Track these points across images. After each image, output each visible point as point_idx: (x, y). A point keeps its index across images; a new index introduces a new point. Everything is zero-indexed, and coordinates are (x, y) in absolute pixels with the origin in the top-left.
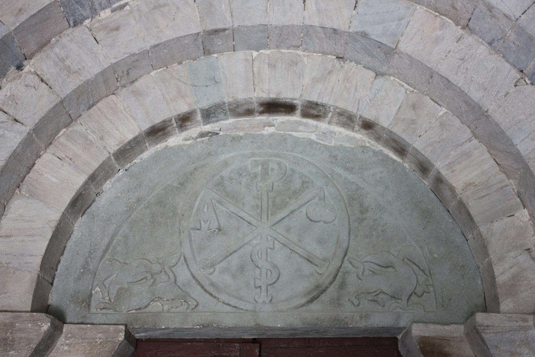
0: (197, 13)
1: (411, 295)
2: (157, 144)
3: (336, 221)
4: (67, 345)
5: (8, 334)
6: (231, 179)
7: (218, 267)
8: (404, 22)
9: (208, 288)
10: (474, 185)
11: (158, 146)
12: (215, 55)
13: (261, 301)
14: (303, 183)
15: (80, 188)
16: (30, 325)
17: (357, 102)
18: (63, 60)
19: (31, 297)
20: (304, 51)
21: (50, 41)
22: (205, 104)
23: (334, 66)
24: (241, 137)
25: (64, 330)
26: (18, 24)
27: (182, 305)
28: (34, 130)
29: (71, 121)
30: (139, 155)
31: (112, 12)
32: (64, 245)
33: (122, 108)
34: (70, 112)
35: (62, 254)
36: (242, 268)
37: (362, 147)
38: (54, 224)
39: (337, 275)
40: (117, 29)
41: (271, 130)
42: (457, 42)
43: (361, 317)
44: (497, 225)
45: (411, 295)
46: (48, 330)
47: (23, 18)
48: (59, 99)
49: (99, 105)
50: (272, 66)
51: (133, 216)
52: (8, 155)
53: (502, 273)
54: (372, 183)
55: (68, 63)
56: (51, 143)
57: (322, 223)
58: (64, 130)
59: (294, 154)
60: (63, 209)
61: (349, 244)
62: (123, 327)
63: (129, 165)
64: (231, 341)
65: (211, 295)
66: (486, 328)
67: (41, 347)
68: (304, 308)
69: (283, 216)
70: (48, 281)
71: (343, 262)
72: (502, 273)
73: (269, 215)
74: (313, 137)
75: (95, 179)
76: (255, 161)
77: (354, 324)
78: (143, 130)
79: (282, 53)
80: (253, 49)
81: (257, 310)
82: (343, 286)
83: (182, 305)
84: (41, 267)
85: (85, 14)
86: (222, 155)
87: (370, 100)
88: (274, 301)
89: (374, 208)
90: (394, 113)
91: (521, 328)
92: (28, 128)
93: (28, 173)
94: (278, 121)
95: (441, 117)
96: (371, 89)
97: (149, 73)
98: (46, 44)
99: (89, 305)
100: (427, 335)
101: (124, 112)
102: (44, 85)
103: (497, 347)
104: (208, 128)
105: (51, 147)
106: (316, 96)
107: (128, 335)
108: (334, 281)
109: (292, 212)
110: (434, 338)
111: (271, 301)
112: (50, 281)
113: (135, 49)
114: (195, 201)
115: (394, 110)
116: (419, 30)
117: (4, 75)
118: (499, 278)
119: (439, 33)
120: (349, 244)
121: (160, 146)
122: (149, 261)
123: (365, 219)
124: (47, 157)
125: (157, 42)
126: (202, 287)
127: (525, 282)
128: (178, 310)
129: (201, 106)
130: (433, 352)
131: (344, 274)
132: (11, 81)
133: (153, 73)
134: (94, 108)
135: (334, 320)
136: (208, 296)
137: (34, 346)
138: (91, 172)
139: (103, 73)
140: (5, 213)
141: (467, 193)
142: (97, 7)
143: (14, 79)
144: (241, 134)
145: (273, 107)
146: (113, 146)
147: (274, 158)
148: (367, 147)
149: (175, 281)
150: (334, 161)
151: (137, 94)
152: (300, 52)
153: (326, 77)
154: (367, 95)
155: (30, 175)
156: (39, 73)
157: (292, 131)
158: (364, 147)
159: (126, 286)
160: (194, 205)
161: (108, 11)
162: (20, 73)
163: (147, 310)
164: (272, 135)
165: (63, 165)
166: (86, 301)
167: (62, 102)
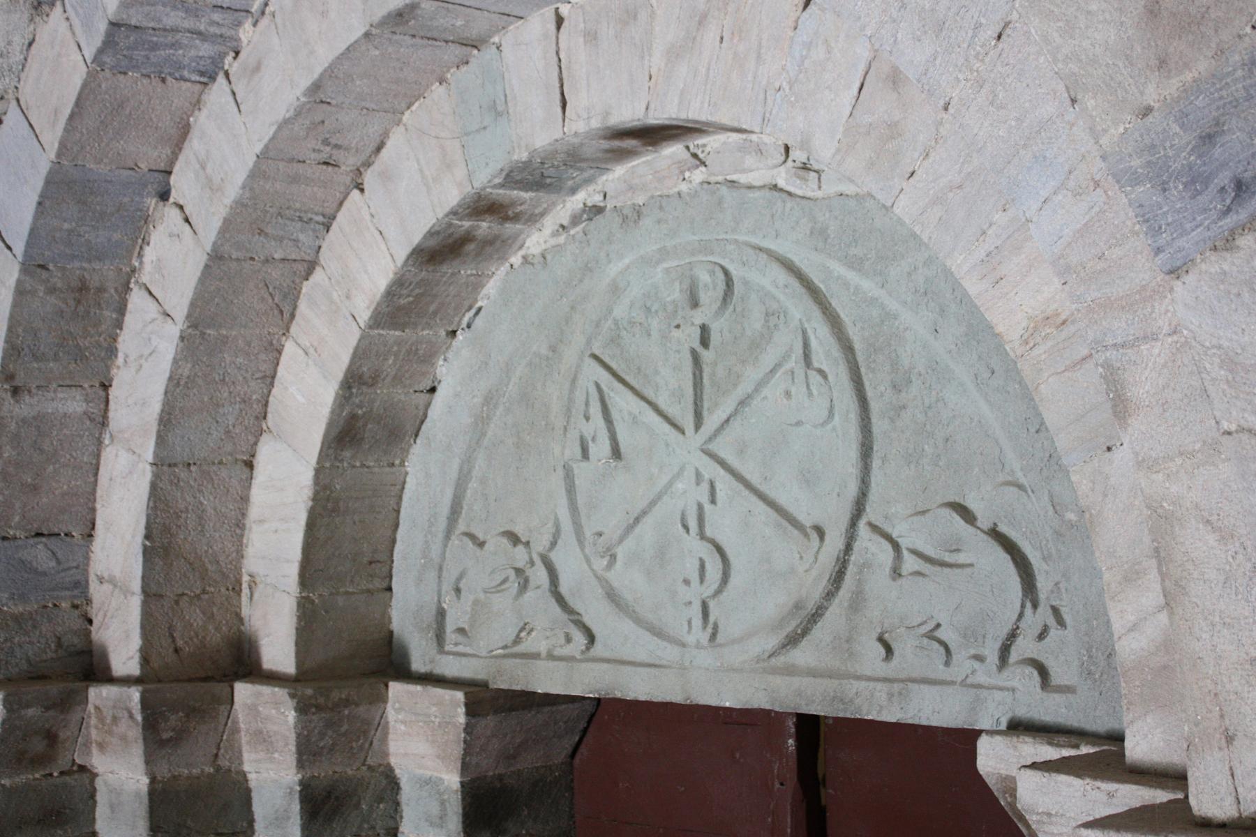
3: (837, 417)
6: (632, 323)
10: (1059, 321)
35: (397, 526)
51: (490, 433)
53: (1134, 628)
54: (909, 299)
66: (1045, 818)
69: (724, 417)
77: (875, 713)
81: (687, 664)
82: (857, 603)
86: (611, 265)
87: (789, 83)
88: (720, 638)
89: (923, 372)
108: (838, 588)
109: (742, 403)
111: (714, 636)
118: (1124, 642)
135: (834, 698)
141: (1036, 352)
150: (821, 245)
153: (694, 38)
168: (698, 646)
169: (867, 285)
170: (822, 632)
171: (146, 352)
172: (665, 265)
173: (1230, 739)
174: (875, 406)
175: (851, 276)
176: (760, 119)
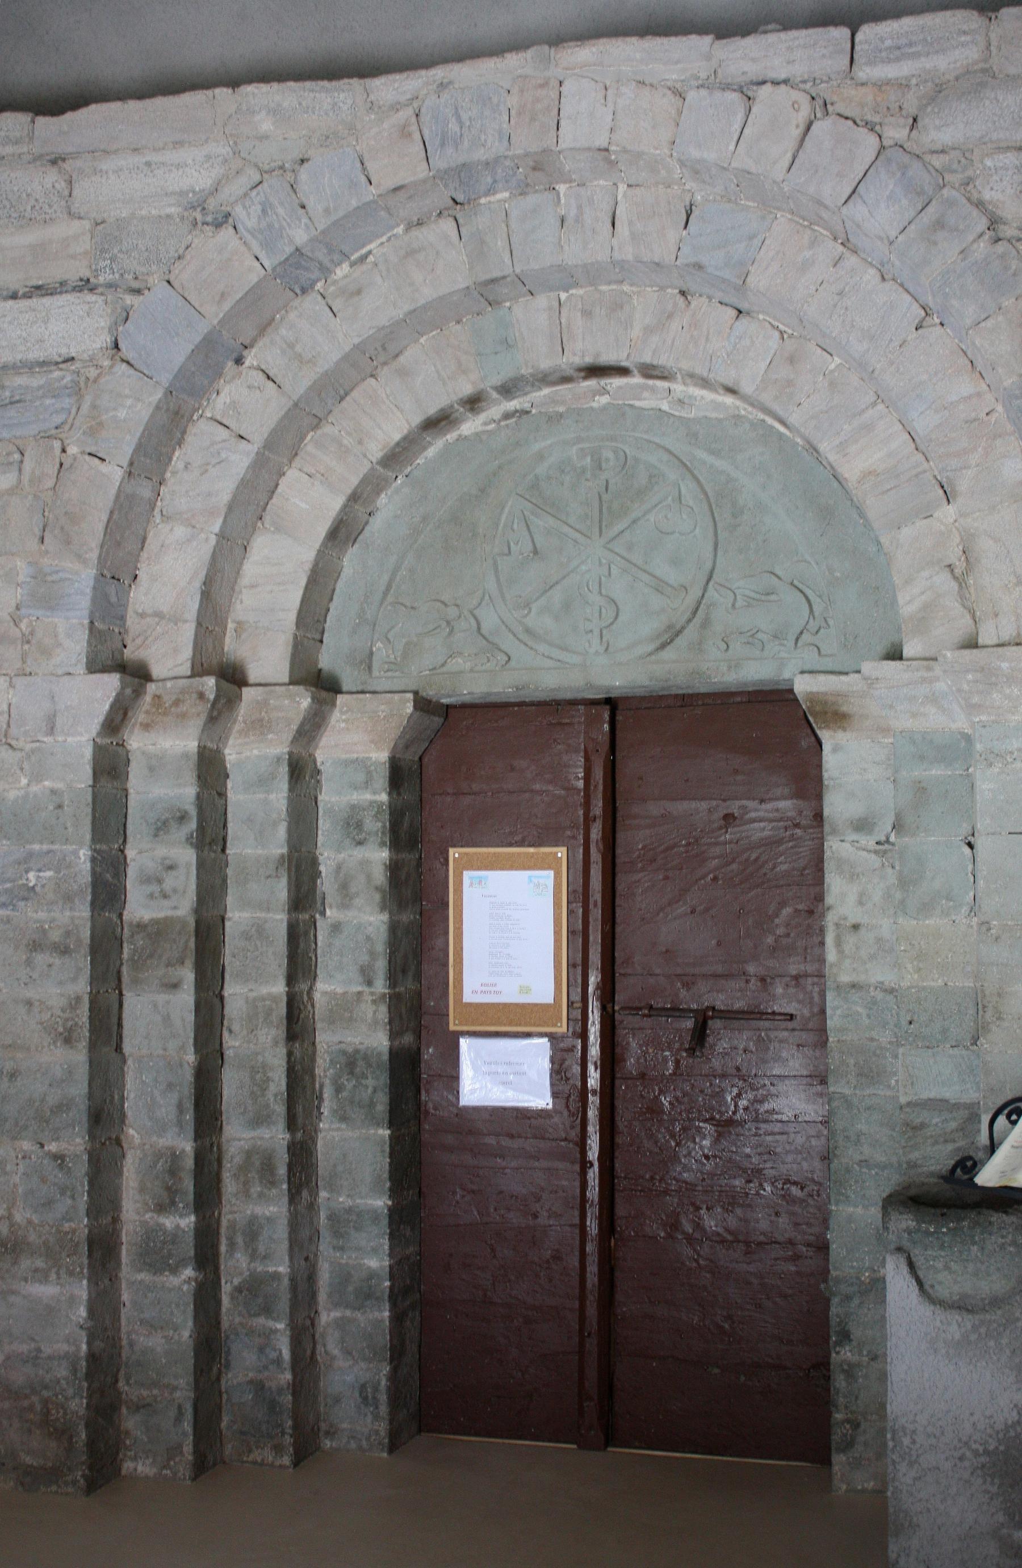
0: (465, 257)
1: (801, 633)
2: (445, 435)
3: (697, 530)
4: (344, 721)
5: (263, 714)
6: (549, 478)
7: (534, 607)
8: (757, 242)
9: (521, 637)
11: (448, 437)
12: (508, 304)
13: (592, 650)
14: (650, 477)
15: (338, 515)
16: (286, 702)
17: (709, 358)
18: (291, 346)
19: (288, 666)
20: (631, 285)
21: (273, 319)
22: (496, 380)
23: (675, 305)
24: (561, 415)
25: (338, 702)
26: (221, 315)
27: (489, 661)
28: (264, 447)
29: (318, 422)
30: (420, 454)
31: (351, 267)
32: (331, 587)
33: (384, 395)
34: (314, 412)
35: (331, 599)
36: (567, 606)
37: (734, 417)
38: (308, 567)
39: (697, 609)
40: (359, 292)
41: (605, 400)
42: (835, 265)
43: (729, 668)
44: (906, 532)
45: (801, 633)
46: (310, 707)
47: (227, 306)
48: (291, 402)
49: (355, 394)
50: (587, 313)
52: (235, 486)
53: (909, 602)
55: (298, 348)
56: (296, 454)
57: (677, 535)
58: (312, 433)
59: (637, 435)
60: (317, 546)
61: (714, 562)
62: (410, 696)
63: (409, 469)
64: (573, 703)
65: (526, 644)
67: (307, 728)
68: (653, 657)
70: (313, 639)
71: (705, 590)
72: (909, 602)
73: (604, 528)
74: (665, 407)
75: (361, 498)
76: (582, 449)
78: (413, 425)
79: (600, 292)
80: (558, 289)
82: (706, 624)
83: (489, 661)
84: (298, 624)
85: (313, 277)
88: (611, 649)
90: (762, 372)
91: (924, 680)
92: (256, 446)
93: (271, 498)
94: (614, 385)
95: (832, 371)
96: (729, 335)
97: (416, 341)
98: (269, 324)
99: (370, 668)
100: (815, 689)
101: (387, 402)
102: (271, 383)
104: (513, 405)
105: (298, 459)
106: (650, 354)
107: (423, 705)
109: (634, 522)
110: (826, 694)
111: (607, 649)
112: (318, 637)
113: (383, 320)
114: (501, 514)
115: (763, 365)
116: (778, 253)
117: (220, 375)
119: (808, 254)
120: (714, 562)
121: (451, 437)
122: (443, 602)
123: (739, 525)
124: (292, 473)
125: (412, 308)
126: (515, 635)
127: (942, 613)
128: (484, 668)
129: (490, 384)
130: (826, 713)
131: (708, 607)
132: (229, 382)
133: (422, 340)
134: (348, 398)
136: (523, 647)
137: (294, 727)
138: (349, 491)
139: (346, 358)
140: (247, 555)
142: (329, 265)
143: (234, 378)
144: (561, 409)
145: (595, 371)
146: (376, 451)
147: (607, 443)
148: (744, 417)
149: (479, 629)
151: (403, 373)
152: (626, 288)
154: (724, 347)
155: (274, 501)
156: (263, 367)
157: (634, 399)
158: (738, 417)
159: (415, 639)
160: (499, 519)
161: (345, 267)
162: (240, 368)
163: (444, 669)
164: (604, 408)
165: (313, 484)
166: (367, 662)
167: (296, 405)
168: (597, 653)
169: (720, 464)
170: (681, 641)
171: (214, 461)
172: (580, 446)
173: (996, 615)
174: (720, 525)
175: (710, 459)
176: (707, 369)
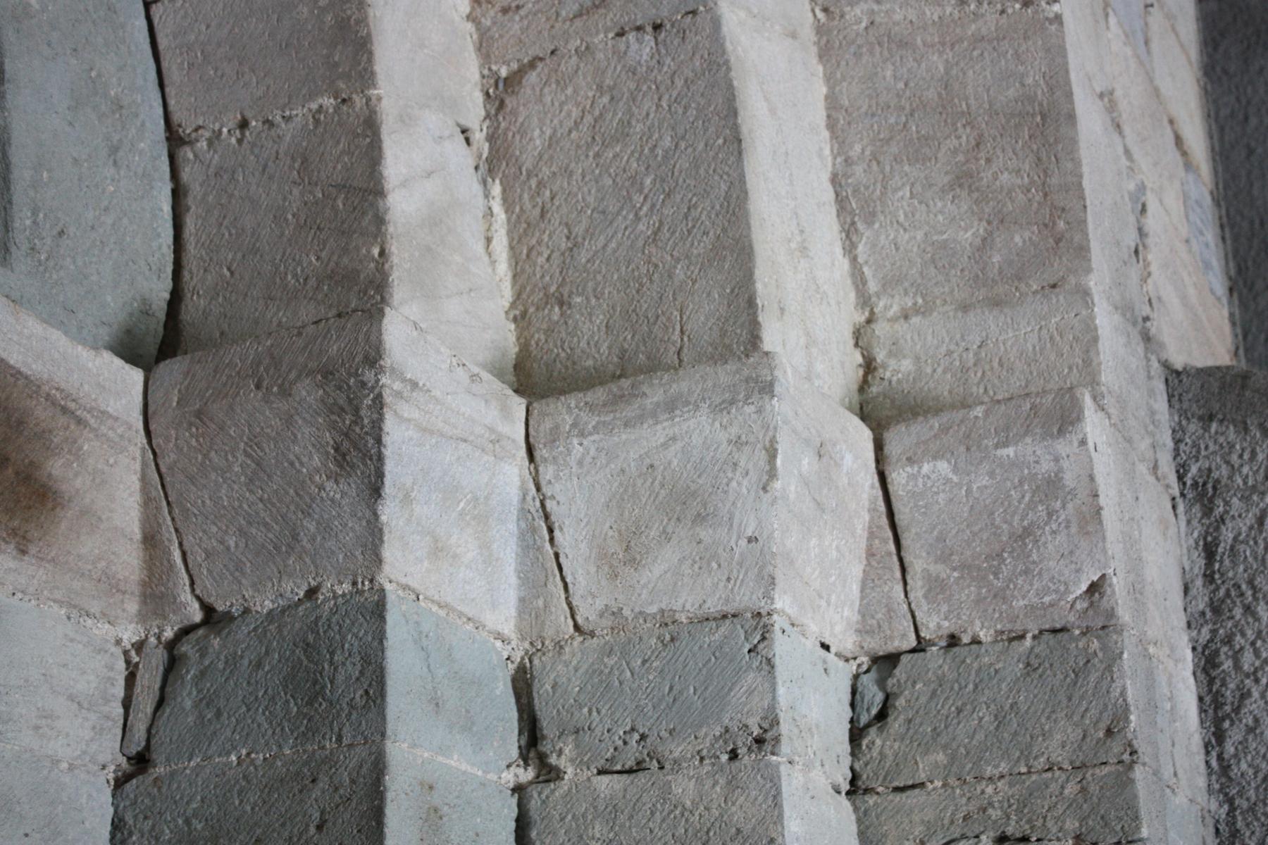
103: (407, 500)
110: (32, 386)
